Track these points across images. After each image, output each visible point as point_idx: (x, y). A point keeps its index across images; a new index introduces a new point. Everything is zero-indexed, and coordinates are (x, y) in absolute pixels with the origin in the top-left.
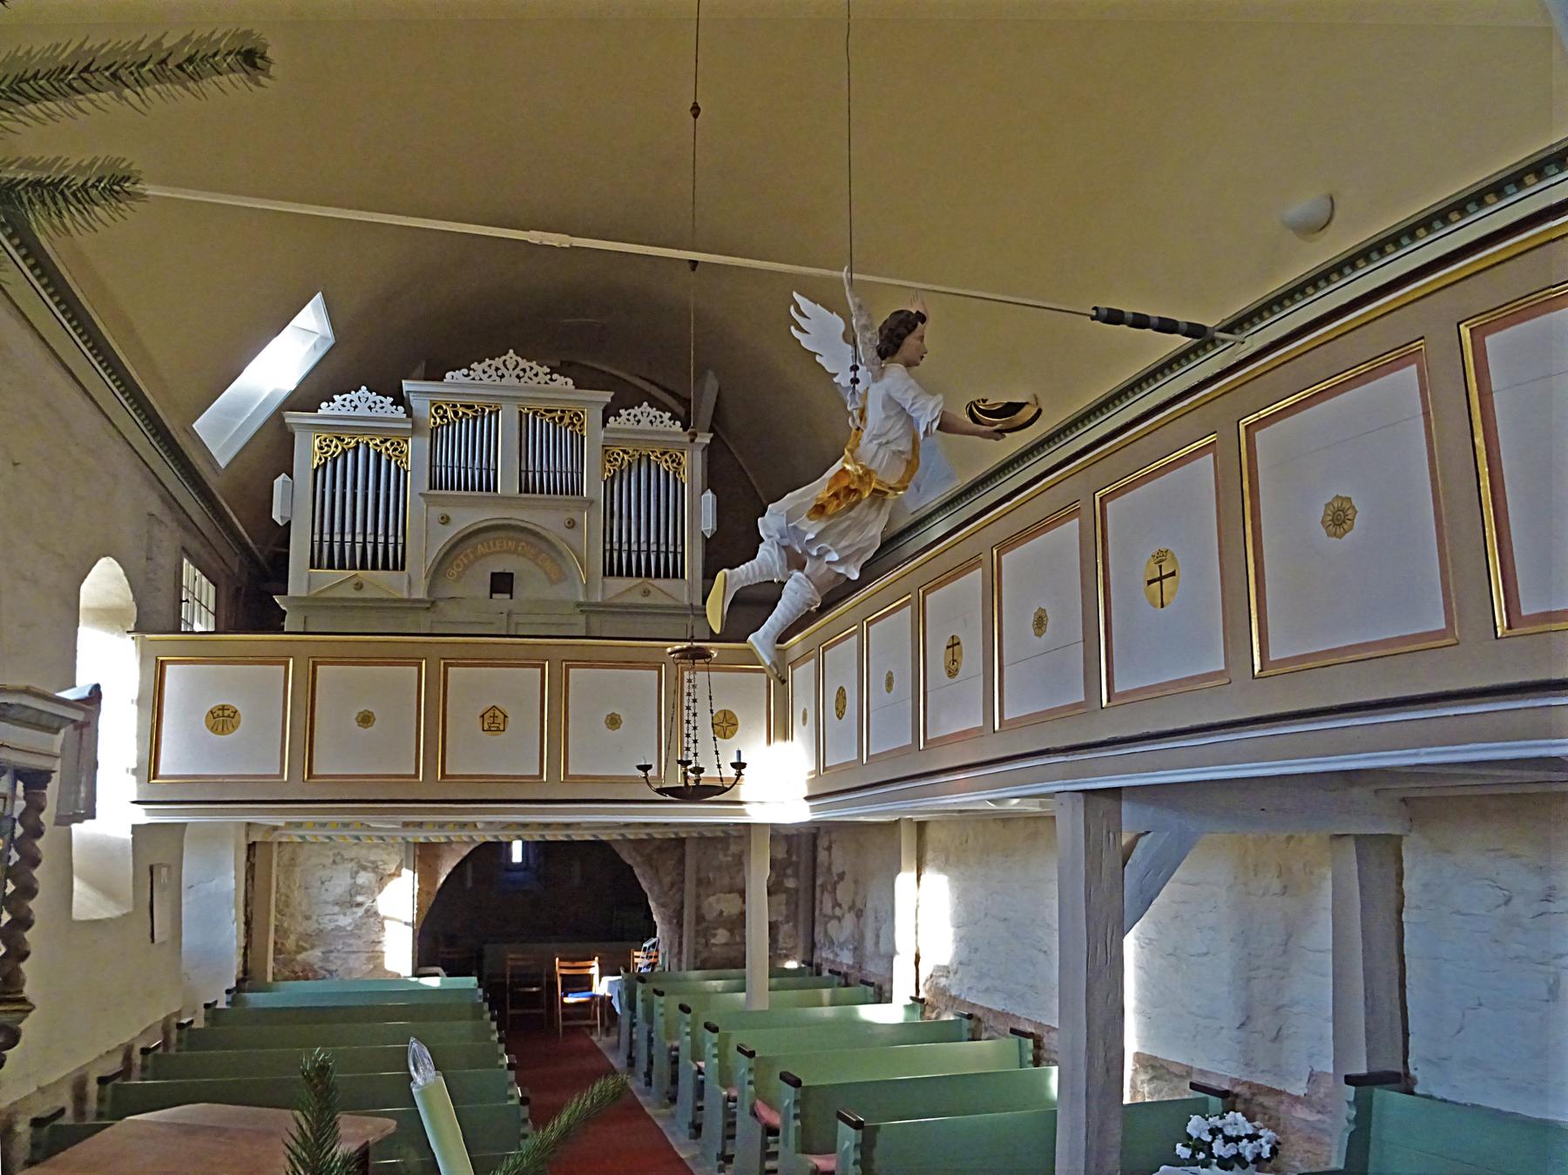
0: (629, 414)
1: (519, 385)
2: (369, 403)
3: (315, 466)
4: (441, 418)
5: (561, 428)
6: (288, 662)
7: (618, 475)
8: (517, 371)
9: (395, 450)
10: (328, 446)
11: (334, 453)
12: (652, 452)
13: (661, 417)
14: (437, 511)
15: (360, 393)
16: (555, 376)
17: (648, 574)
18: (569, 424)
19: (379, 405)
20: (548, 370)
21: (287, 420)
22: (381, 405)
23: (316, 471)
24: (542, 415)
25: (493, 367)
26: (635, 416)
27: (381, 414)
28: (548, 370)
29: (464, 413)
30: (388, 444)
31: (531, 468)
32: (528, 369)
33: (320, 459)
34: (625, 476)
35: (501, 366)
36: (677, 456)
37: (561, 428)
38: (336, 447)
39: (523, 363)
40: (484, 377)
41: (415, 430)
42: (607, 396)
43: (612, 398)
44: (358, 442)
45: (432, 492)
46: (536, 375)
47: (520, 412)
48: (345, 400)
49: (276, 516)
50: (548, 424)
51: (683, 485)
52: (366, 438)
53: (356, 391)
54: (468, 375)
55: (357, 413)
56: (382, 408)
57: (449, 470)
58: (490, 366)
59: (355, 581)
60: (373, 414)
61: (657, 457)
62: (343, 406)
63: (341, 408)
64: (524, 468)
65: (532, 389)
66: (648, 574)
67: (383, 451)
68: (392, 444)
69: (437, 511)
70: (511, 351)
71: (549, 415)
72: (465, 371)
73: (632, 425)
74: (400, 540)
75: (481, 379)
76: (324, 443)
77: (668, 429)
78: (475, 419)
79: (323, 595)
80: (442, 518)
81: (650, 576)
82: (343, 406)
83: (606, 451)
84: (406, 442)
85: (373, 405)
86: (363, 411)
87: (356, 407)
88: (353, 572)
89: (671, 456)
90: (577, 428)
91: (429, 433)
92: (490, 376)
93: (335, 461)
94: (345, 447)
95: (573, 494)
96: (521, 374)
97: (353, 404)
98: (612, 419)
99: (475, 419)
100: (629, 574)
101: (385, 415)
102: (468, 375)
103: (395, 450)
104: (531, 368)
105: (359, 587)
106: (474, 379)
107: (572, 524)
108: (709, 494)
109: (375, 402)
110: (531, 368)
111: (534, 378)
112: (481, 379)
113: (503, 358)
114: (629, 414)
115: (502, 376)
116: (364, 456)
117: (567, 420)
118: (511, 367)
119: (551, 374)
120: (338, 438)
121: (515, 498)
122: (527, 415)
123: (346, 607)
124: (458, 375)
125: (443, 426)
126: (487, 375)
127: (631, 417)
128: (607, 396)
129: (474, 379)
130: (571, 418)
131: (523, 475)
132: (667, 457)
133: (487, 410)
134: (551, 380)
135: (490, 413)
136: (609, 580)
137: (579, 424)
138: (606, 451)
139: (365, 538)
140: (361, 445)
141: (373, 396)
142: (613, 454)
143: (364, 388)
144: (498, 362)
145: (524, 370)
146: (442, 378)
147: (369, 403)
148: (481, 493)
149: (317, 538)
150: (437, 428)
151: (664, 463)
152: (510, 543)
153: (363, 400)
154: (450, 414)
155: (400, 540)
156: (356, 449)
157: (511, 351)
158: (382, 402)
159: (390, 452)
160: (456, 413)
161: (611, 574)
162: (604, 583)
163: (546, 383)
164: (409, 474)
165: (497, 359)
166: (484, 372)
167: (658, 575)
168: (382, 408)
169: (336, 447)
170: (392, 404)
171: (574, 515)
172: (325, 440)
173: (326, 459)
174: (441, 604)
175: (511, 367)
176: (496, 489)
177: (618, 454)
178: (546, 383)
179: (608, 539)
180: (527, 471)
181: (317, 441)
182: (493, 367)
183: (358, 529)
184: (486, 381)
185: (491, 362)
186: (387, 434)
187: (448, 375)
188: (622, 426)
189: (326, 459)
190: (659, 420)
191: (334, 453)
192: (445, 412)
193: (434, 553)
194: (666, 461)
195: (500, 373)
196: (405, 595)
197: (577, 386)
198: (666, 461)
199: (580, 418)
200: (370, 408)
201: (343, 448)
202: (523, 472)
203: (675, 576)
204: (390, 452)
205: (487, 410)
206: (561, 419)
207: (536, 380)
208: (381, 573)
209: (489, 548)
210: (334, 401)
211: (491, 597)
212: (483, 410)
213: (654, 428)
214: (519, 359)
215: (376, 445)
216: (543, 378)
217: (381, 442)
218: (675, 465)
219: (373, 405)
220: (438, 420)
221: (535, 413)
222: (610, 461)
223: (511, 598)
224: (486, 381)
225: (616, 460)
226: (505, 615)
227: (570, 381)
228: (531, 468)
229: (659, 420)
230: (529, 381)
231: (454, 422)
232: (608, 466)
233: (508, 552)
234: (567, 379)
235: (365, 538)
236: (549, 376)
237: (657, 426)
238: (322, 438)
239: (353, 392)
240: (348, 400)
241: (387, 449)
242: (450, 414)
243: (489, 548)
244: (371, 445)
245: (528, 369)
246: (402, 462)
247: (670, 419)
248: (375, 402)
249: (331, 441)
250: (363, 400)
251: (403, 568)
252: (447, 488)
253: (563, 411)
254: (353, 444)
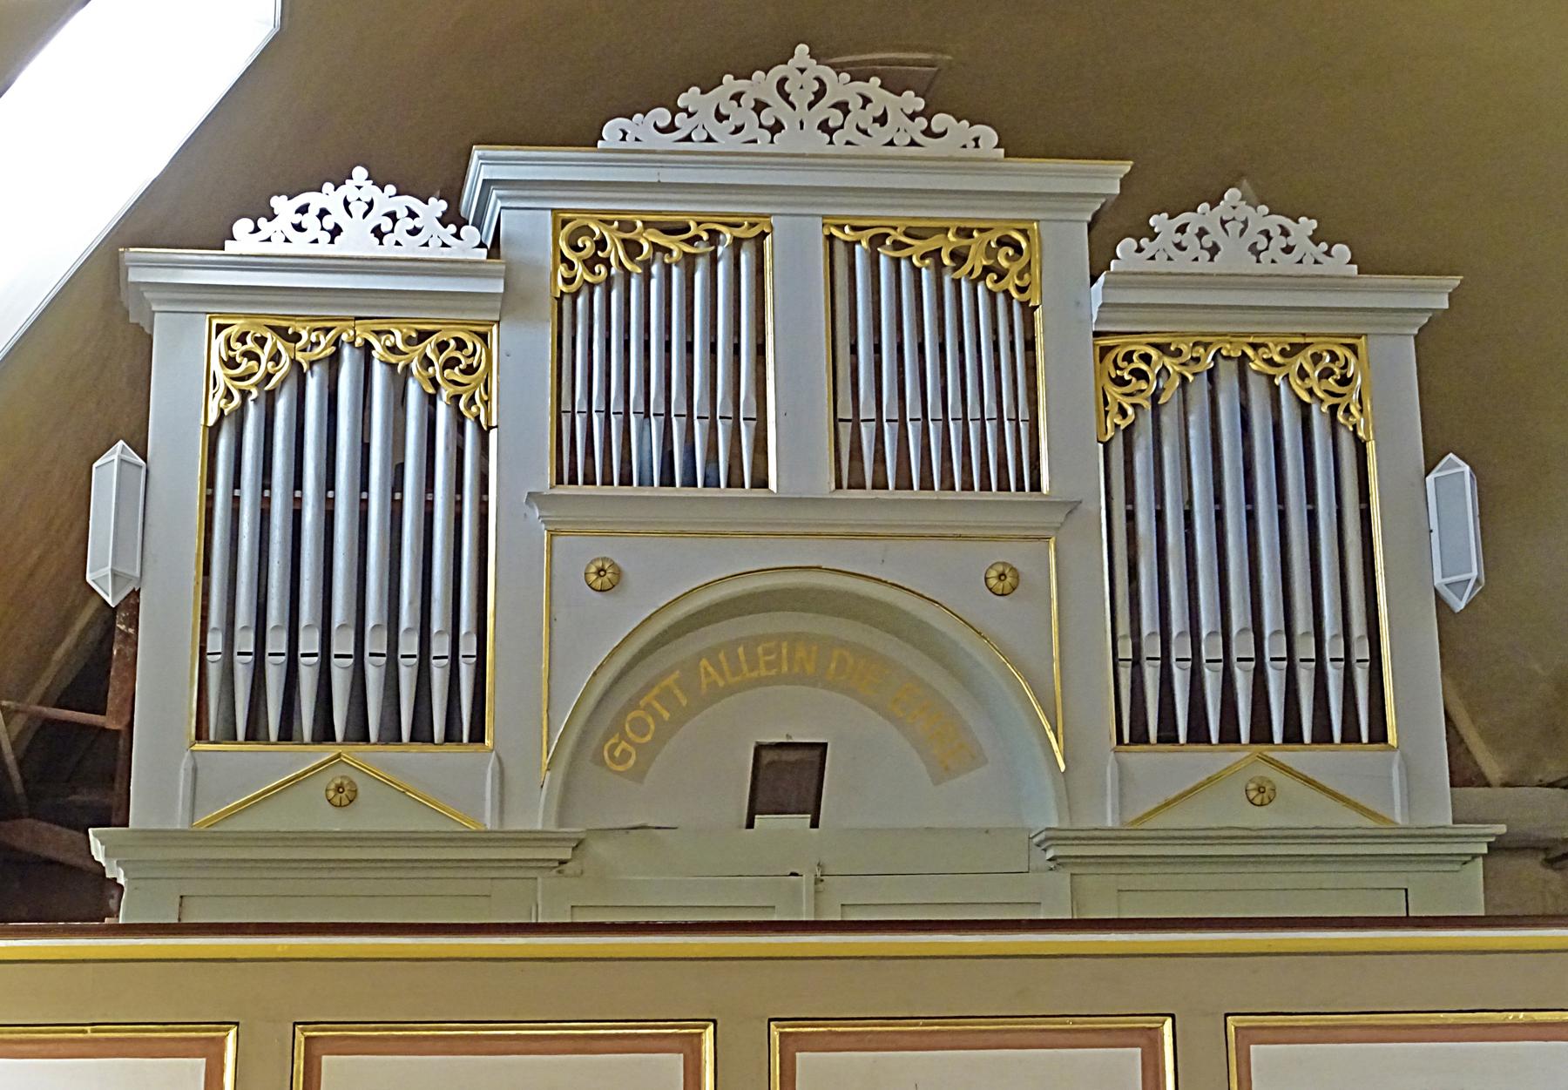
0: (303, 210)
1: (830, 149)
2: (376, 217)
3: (213, 418)
4: (590, 264)
5: (957, 283)
6: (221, 1042)
7: (1146, 422)
8: (823, 110)
9: (1326, 374)
10: (251, 356)
11: (269, 376)
12: (1255, 347)
13: (1285, 233)
14: (580, 553)
15: (348, 189)
16: (941, 121)
17: (1261, 734)
18: (987, 270)
19: (405, 223)
20: (920, 104)
21: (135, 276)
22: (411, 224)
23: (213, 433)
24: (898, 245)
25: (748, 102)
26: (1202, 233)
27: (411, 248)
28: (920, 104)
29: (655, 246)
30: (429, 347)
31: (867, 410)
32: (855, 104)
33: (229, 395)
34: (1169, 421)
35: (774, 98)
36: (1334, 357)
37: (957, 283)
38: (276, 358)
39: (841, 86)
40: (721, 131)
41: (512, 302)
42: (1108, 178)
43: (1124, 182)
44: (337, 342)
45: (566, 490)
46: (882, 120)
47: (831, 238)
48: (303, 210)
49: (99, 575)
50: (917, 271)
51: (1361, 447)
52: (363, 334)
53: (1214, 205)
54: (672, 128)
55: (342, 247)
56: (414, 232)
57: (990, 428)
58: (737, 97)
59: (332, 778)
60: (388, 250)
61: (1270, 362)
62: (1179, 246)
63: (1174, 252)
64: (846, 412)
65: (871, 162)
66: (1261, 734)
67: (415, 366)
68: (442, 346)
69: (580, 553)
70: (802, 49)
71: (920, 246)
72: (662, 116)
73: (1192, 261)
74: (468, 646)
75: (709, 139)
76: (238, 347)
77: (1308, 268)
78: (689, 261)
79: (240, 825)
80: (600, 572)
81: (1174, 740)
82: (298, 228)
83: (1105, 351)
84: (484, 337)
85: (386, 225)
86: (357, 241)
87: (336, 231)
88: (327, 752)
89: (1317, 358)
90: (1011, 283)
91: (549, 309)
92: (738, 130)
93: (271, 398)
94: (299, 357)
95: (1003, 486)
96: (836, 117)
97: (329, 222)
98: (1125, 247)
99: (689, 261)
100: (1198, 734)
101: (424, 253)
102: (672, 128)
103: (451, 363)
104: (867, 101)
105: (345, 796)
106: (688, 138)
107: (1008, 583)
108: (1456, 468)
109: (392, 216)
110: (867, 101)
111: (875, 129)
112: (709, 139)
113: (778, 72)
114: (1182, 229)
115: (777, 127)
116: (355, 383)
117: (977, 261)
118: (802, 98)
119: (928, 114)
120: (281, 332)
121: (816, 502)
122: (851, 246)
123: (1100, 863)
124: (642, 129)
125: (591, 286)
126: (729, 125)
127: (1189, 238)
128: (1108, 178)
129: (688, 138)
130: (990, 253)
131: (846, 430)
132: (1303, 359)
133: (727, 235)
134: (928, 132)
135: (737, 243)
136: (1138, 757)
137: (1015, 268)
138: (1105, 351)
139: (1137, 649)
140: (346, 351)
141: (387, 199)
142: (1128, 357)
143: (360, 173)
144: (762, 84)
145: (843, 107)
146: (593, 138)
147: (376, 217)
148: (689, 492)
149: (215, 642)
150: (575, 296)
151: (1296, 382)
152: (801, 653)
153: (358, 208)
154: (614, 251)
155: (468, 646)
156: (334, 360)
157: (802, 49)
158: (412, 215)
159: (435, 370)
160: (632, 248)
161: (1140, 737)
162: (1121, 766)
163: (913, 143)
164: (493, 434)
165: (758, 74)
166: (720, 117)
167: (1293, 735)
168: (414, 232)
169: (276, 358)
170: (1315, 239)
171: (1016, 554)
172: (242, 339)
173: (245, 394)
174: (600, 849)
175: (802, 98)
176: (1036, 486)
177: (1146, 358)
178: (913, 143)
179: (215, 619)
180: (856, 423)
181: (218, 343)
182: (748, 102)
183: (1178, 623)
184: (726, 141)
185: (742, 84)
186: (426, 317)
187: (611, 129)
188: (1160, 265)
189: (245, 394)
190: (1279, 242)
191: (269, 376)
192: (601, 244)
193: (577, 685)
194: (1303, 375)
195: (767, 118)
196: (489, 822)
197: (1012, 147)
198: (1303, 375)
199: (1018, 249)
200: (378, 232)
201: (295, 363)
202: (845, 423)
203: (1351, 735)
204: (435, 370)
205: (727, 235)
206: (959, 257)
207: (880, 134)
208: (409, 754)
209: (736, 671)
210: (271, 216)
211: (750, 825)
212: (714, 235)
213: (1265, 267)
214: (828, 74)
215: (393, 349)
216: (903, 129)
217: (408, 341)
218: (455, 374)
219: (386, 225)
220: (579, 268)
221: (877, 241)
222: (1119, 381)
223: (814, 824)
224: (726, 141)
225: (1140, 375)
226: (806, 882)
227: (989, 136)
228: (867, 410)
229: (1279, 242)
230: (858, 137)
231: (628, 275)
232: (1114, 392)
233: (800, 679)
234: (980, 129)
235: (1137, 649)
236: (922, 122)
237: (1276, 262)
238: (234, 331)
239: (328, 187)
240: (314, 211)
241: (427, 362)
242: (614, 251)
243: (736, 671)
244: (378, 352)
245: (855, 104)
246: (472, 400)
247: (1315, 239)
248: (392, 216)
249: (261, 342)
250: (358, 208)
251: (478, 735)
252: (607, 481)
253: (966, 233)
254: (324, 350)
